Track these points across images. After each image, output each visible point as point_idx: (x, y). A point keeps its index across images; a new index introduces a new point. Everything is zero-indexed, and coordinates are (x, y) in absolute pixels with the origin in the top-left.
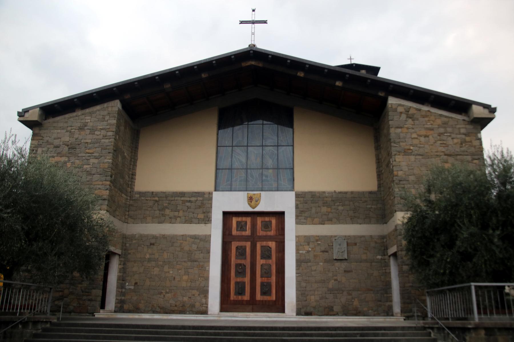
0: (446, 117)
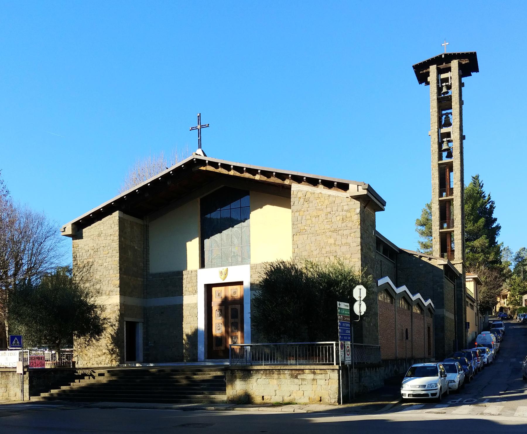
0: (333, 196)
